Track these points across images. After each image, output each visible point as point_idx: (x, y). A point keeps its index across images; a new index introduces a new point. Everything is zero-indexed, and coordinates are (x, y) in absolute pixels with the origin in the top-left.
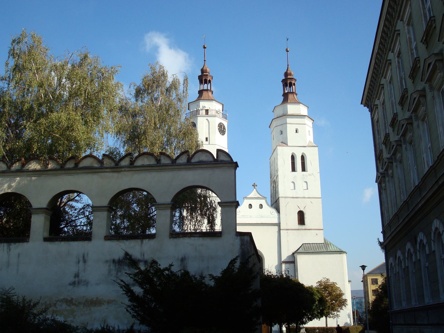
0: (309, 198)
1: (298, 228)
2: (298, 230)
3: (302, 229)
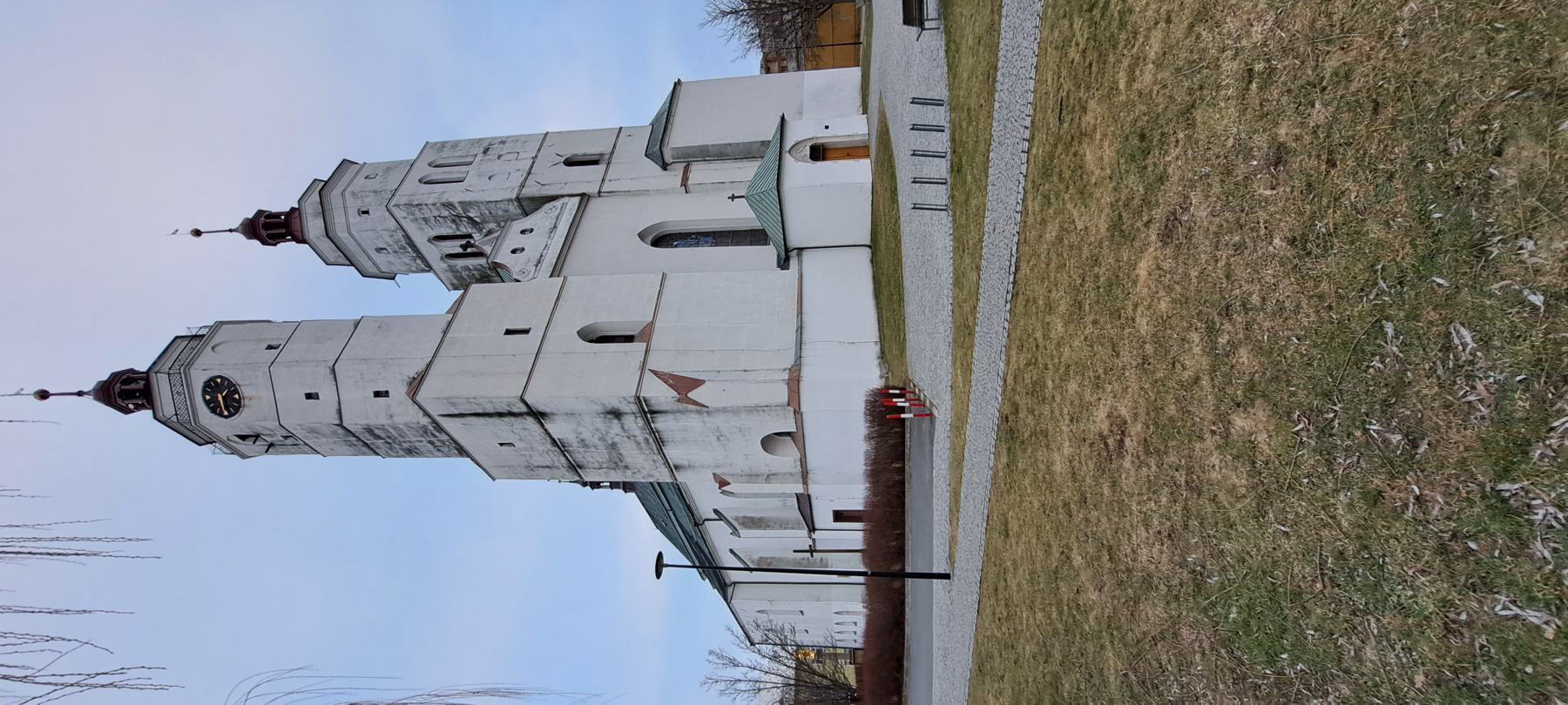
0: (539, 150)
1: (605, 166)
3: (610, 158)
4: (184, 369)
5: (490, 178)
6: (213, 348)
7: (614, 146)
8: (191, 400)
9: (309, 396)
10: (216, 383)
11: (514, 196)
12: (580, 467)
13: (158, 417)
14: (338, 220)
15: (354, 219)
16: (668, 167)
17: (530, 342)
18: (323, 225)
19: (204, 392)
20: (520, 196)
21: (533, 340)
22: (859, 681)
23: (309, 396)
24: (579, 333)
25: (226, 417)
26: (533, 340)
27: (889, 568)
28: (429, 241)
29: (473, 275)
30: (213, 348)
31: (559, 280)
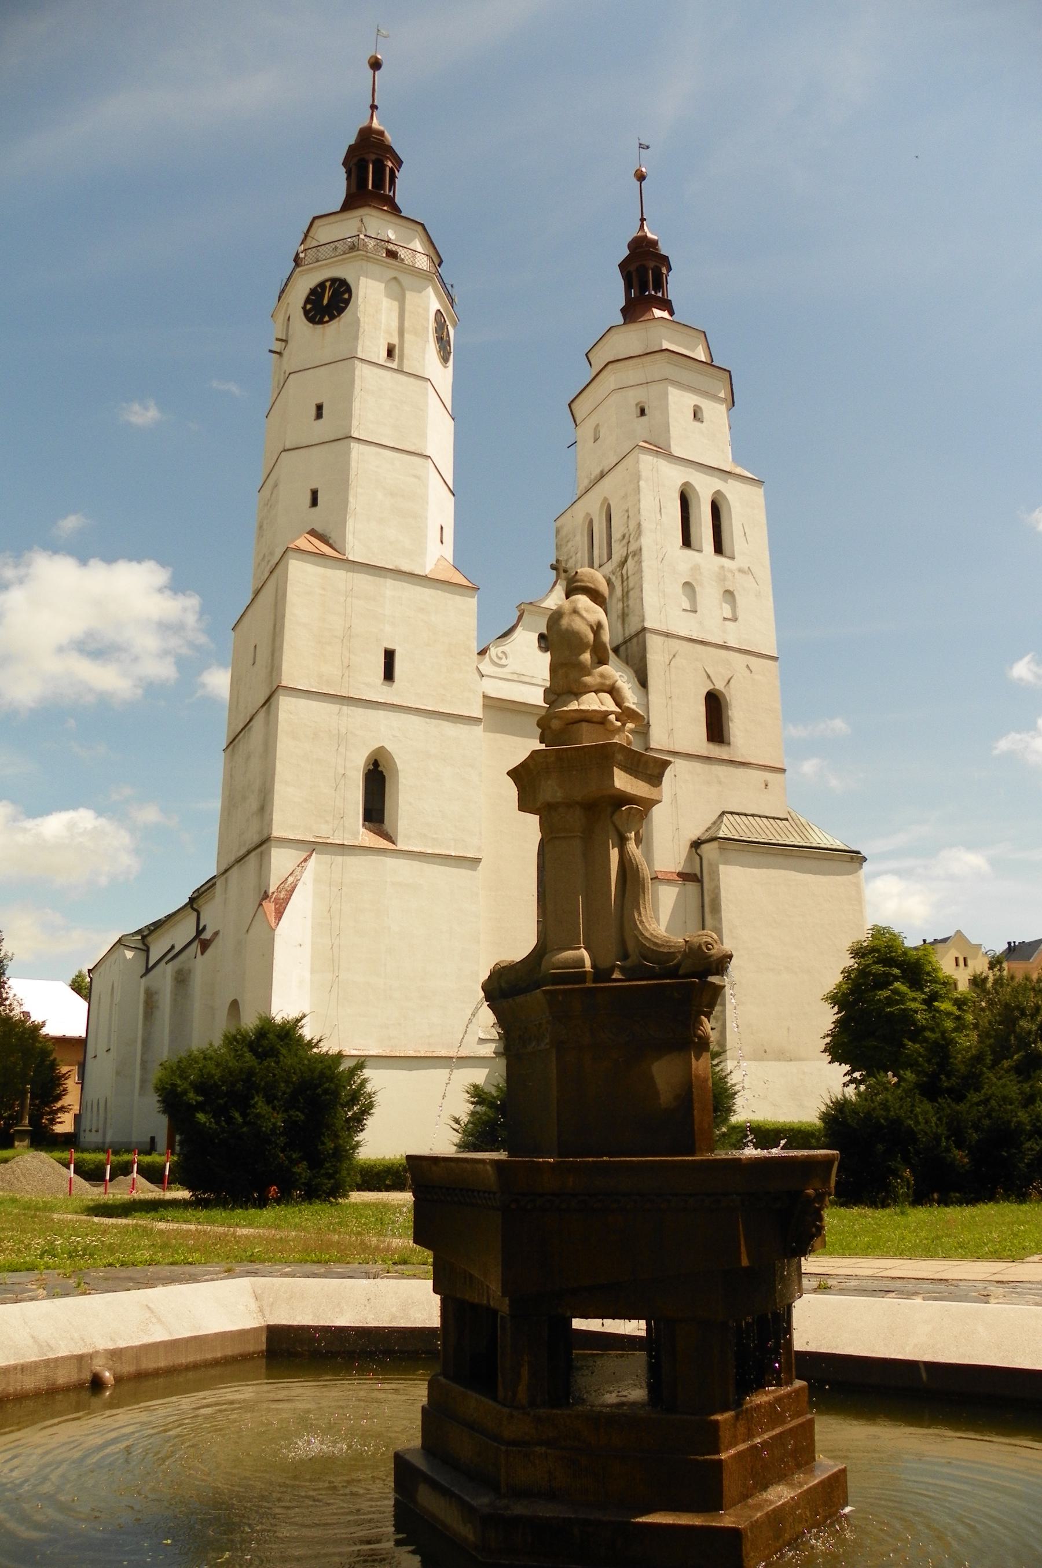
2: (708, 759)
4: (363, 255)
5: (687, 584)
6: (395, 278)
7: (744, 764)
8: (326, 265)
9: (319, 408)
10: (344, 293)
11: (647, 625)
12: (233, 750)
13: (316, 221)
14: (630, 374)
15: (633, 397)
16: (693, 849)
17: (375, 689)
18: (621, 358)
19: (334, 280)
20: (648, 635)
21: (381, 692)
22: (711, 1420)
23: (319, 408)
24: (381, 750)
25: (304, 308)
26: (381, 692)
27: (821, 1451)
28: (606, 499)
29: (571, 557)
30: (395, 278)
31: (477, 712)
